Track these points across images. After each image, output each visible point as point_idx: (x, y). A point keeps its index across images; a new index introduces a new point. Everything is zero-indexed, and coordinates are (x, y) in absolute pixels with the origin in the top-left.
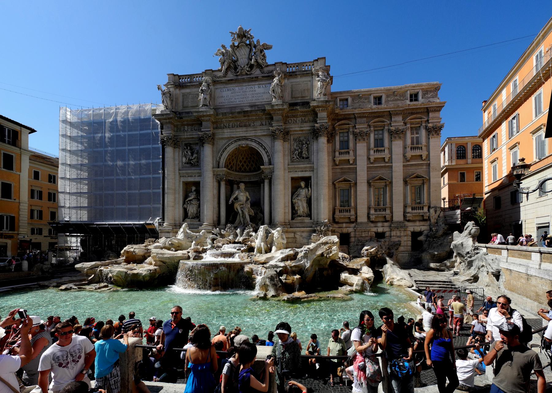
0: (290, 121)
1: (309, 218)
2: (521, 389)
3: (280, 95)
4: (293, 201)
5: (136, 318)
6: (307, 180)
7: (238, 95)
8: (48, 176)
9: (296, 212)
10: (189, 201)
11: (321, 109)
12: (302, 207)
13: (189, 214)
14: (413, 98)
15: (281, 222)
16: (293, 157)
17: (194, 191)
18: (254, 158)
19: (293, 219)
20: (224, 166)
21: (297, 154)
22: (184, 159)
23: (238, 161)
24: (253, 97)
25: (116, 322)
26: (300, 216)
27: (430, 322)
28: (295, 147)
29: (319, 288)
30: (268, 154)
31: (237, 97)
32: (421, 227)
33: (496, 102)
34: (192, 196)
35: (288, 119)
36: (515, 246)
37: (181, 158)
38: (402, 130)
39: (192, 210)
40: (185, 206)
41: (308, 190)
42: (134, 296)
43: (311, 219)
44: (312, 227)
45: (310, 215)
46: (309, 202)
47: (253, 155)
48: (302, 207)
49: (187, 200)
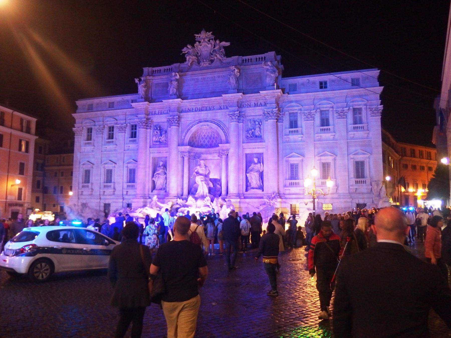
0: (245, 106)
1: (262, 190)
2: (74, 236)
4: (247, 174)
8: (19, 120)
9: (250, 184)
10: (157, 174)
11: (270, 96)
12: (254, 179)
13: (157, 187)
15: (235, 194)
16: (248, 136)
17: (162, 165)
18: (214, 135)
19: (247, 190)
20: (187, 144)
25: (184, 110)
26: (253, 188)
30: (225, 133)
34: (160, 171)
36: (93, 248)
37: (152, 137)
39: (159, 182)
40: (154, 179)
43: (263, 191)
45: (261, 188)
46: (261, 175)
47: (213, 133)
48: (254, 179)
49: (156, 174)
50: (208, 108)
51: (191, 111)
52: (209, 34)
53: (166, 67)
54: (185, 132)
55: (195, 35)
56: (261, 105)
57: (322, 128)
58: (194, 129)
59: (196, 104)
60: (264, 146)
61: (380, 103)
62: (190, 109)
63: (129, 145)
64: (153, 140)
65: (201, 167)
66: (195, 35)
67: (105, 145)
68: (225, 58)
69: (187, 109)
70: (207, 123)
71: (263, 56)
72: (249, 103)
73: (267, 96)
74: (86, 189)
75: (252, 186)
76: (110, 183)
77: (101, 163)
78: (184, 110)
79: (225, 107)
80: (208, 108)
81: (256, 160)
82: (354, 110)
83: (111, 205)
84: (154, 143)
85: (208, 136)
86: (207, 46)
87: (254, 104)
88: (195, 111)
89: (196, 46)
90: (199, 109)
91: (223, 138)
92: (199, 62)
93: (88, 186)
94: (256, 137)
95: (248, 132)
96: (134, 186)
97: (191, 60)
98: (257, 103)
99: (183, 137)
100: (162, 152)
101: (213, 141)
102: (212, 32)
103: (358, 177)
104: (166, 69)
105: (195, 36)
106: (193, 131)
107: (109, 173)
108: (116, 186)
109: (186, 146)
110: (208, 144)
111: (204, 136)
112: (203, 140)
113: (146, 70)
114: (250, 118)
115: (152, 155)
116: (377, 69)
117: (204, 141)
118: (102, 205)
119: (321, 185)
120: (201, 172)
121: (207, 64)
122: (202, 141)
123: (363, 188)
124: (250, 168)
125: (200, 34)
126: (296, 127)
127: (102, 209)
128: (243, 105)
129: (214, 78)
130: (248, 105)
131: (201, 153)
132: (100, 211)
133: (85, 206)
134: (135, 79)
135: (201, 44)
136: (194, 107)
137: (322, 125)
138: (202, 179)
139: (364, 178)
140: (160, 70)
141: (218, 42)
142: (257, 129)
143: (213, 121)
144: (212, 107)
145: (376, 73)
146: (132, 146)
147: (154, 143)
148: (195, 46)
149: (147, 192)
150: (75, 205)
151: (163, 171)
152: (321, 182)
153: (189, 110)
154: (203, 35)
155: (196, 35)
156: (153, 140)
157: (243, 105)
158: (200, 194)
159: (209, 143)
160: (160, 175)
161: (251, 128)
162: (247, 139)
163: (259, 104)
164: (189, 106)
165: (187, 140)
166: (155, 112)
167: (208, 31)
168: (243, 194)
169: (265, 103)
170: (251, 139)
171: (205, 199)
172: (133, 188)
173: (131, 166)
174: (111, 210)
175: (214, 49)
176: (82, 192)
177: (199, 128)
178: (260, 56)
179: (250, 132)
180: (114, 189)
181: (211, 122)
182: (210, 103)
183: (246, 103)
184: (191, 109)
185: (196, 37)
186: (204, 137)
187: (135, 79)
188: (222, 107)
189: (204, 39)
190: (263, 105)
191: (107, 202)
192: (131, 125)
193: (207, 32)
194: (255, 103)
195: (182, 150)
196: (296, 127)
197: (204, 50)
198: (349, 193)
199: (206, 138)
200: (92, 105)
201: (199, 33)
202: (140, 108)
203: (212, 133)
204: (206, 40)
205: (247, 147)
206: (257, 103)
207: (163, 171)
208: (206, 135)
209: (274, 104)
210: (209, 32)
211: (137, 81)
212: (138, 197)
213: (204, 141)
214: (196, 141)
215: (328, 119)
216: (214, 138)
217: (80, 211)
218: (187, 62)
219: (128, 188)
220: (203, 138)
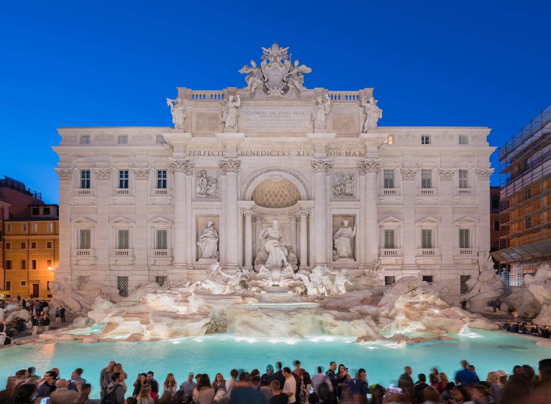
0: (333, 154)
3: (323, 124)
5: (83, 376)
6: (352, 220)
7: (269, 120)
10: (205, 237)
11: (371, 143)
12: (344, 247)
14: (425, 141)
16: (335, 193)
18: (283, 192)
21: (339, 190)
22: (198, 189)
23: (264, 195)
24: (288, 123)
25: (245, 153)
27: (278, 367)
28: (336, 182)
29: (519, 331)
31: (267, 122)
32: (469, 270)
33: (543, 149)
35: (330, 151)
38: (453, 172)
41: (353, 230)
42: (538, 344)
44: (358, 269)
46: (353, 241)
48: (344, 247)
50: (281, 153)
51: (256, 154)
52: (283, 50)
53: (214, 92)
54: (247, 183)
55: (262, 48)
56: (354, 155)
57: (424, 189)
58: (259, 180)
59: (264, 146)
60: (357, 207)
61: (490, 166)
62: (253, 152)
63: (155, 197)
64: (196, 191)
65: (274, 229)
66: (262, 48)
67: (113, 195)
68: (305, 88)
69: (250, 152)
70: (281, 173)
71: (356, 93)
72: (339, 151)
73: (367, 142)
74: (85, 257)
75: (341, 255)
76: (128, 248)
77: (109, 221)
78: (245, 153)
79: (306, 154)
80: (281, 153)
81: (346, 223)
82: (460, 171)
83: (129, 278)
84: (199, 196)
85: (274, 192)
86: (278, 69)
87: (345, 153)
88: (262, 155)
89: (262, 64)
90: (267, 154)
91: (303, 193)
92: (266, 90)
93: (88, 253)
94: (347, 195)
95: (335, 189)
96: (166, 253)
97: (255, 84)
98: (350, 152)
99: (244, 190)
100: (213, 208)
101: (279, 200)
102: (288, 48)
103: (461, 246)
104: (214, 95)
105: (263, 50)
106: (259, 182)
107: (124, 236)
108: (136, 253)
109: (249, 200)
110: (272, 202)
111: (269, 192)
112: (267, 198)
113: (181, 90)
114: (338, 171)
115: (195, 212)
116: (487, 127)
117: (268, 200)
118: (115, 279)
119: (422, 255)
120: (273, 235)
121: (278, 93)
122: (265, 199)
123: (467, 259)
124: (338, 233)
125: (270, 48)
126: (392, 186)
127: (115, 284)
128: (330, 152)
129: (288, 113)
130: (338, 154)
131: (264, 214)
132: (112, 286)
133: (84, 280)
134: (167, 99)
135: (270, 64)
136: (261, 151)
137: (424, 186)
138: (275, 244)
139: (430, 248)
140: (204, 96)
141: (296, 63)
142: (348, 185)
143: (288, 171)
144: (287, 153)
145: (487, 131)
146: (160, 199)
147: (199, 196)
148: (262, 66)
149: (189, 262)
150: (66, 279)
151: (213, 233)
152: (422, 251)
153: (252, 154)
154: (275, 51)
155: (264, 49)
156: (196, 191)
157: (330, 152)
158: (272, 263)
159: (273, 202)
160: (208, 239)
161: (338, 183)
162: (334, 197)
163: (352, 153)
164: (253, 148)
165: (249, 194)
166: (199, 152)
167: (283, 45)
168: (192, 264)
169: (360, 154)
170: (340, 197)
171: (285, 269)
172: (165, 255)
173: (160, 227)
174: (129, 285)
175: (290, 73)
176: (78, 260)
177: (268, 179)
178: (352, 93)
179: (337, 188)
180: (133, 256)
181: (286, 171)
182: (285, 146)
183: (334, 151)
184: (256, 153)
185: (264, 52)
186: (268, 193)
187: (167, 99)
188: (301, 153)
189: (275, 58)
190: (357, 155)
191: (122, 274)
192: (157, 170)
193: (281, 48)
194: (346, 152)
195: (242, 207)
196: (392, 186)
197: (273, 74)
198: (147, 265)
199: (271, 196)
200: (88, 137)
201: (269, 46)
202: (176, 142)
203: (280, 188)
204: (279, 59)
205: (335, 207)
206: (350, 152)
207: (213, 233)
208: (271, 191)
209: (376, 154)
210: (284, 48)
211: (169, 102)
212: (178, 267)
213: (268, 200)
214: (258, 197)
215: (430, 180)
216: (281, 196)
217: (75, 288)
218: (248, 87)
219: (156, 256)
220: (266, 195)
